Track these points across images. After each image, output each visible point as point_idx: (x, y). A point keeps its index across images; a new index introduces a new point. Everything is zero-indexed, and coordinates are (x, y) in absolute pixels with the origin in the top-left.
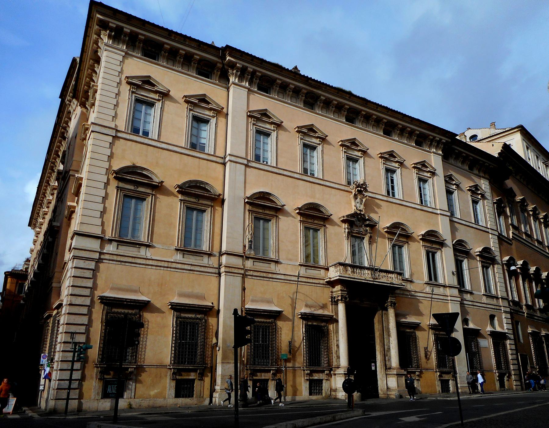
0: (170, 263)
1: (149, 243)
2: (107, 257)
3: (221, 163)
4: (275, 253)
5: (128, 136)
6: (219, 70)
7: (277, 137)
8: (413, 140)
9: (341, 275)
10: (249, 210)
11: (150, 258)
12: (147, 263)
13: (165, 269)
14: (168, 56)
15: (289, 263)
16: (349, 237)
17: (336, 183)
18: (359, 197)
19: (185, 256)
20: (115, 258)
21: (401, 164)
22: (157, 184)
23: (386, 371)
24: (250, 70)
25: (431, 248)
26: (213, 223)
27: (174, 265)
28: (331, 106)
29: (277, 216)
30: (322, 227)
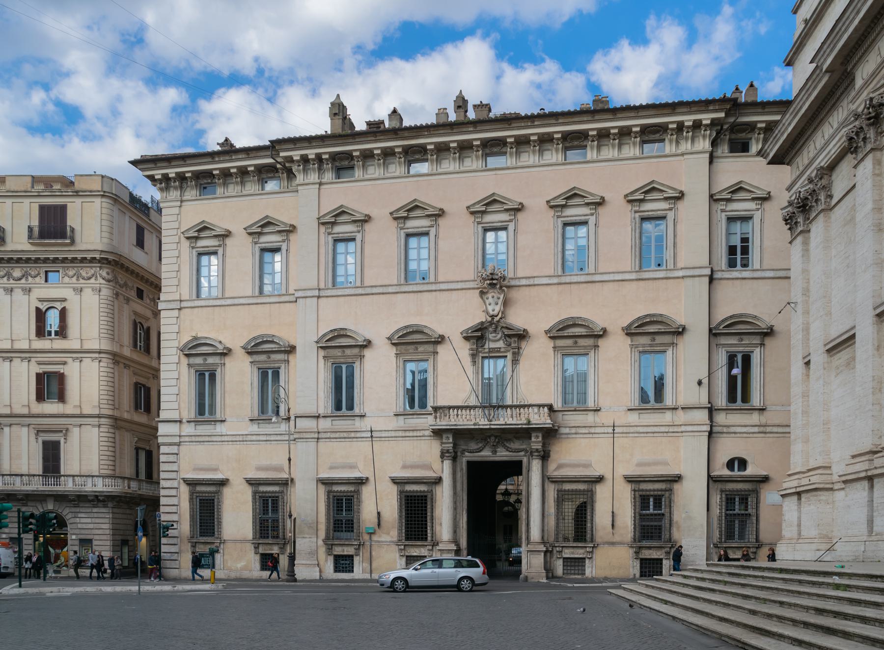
12: (223, 439)
13: (241, 443)
19: (261, 425)
20: (193, 439)
27: (249, 438)
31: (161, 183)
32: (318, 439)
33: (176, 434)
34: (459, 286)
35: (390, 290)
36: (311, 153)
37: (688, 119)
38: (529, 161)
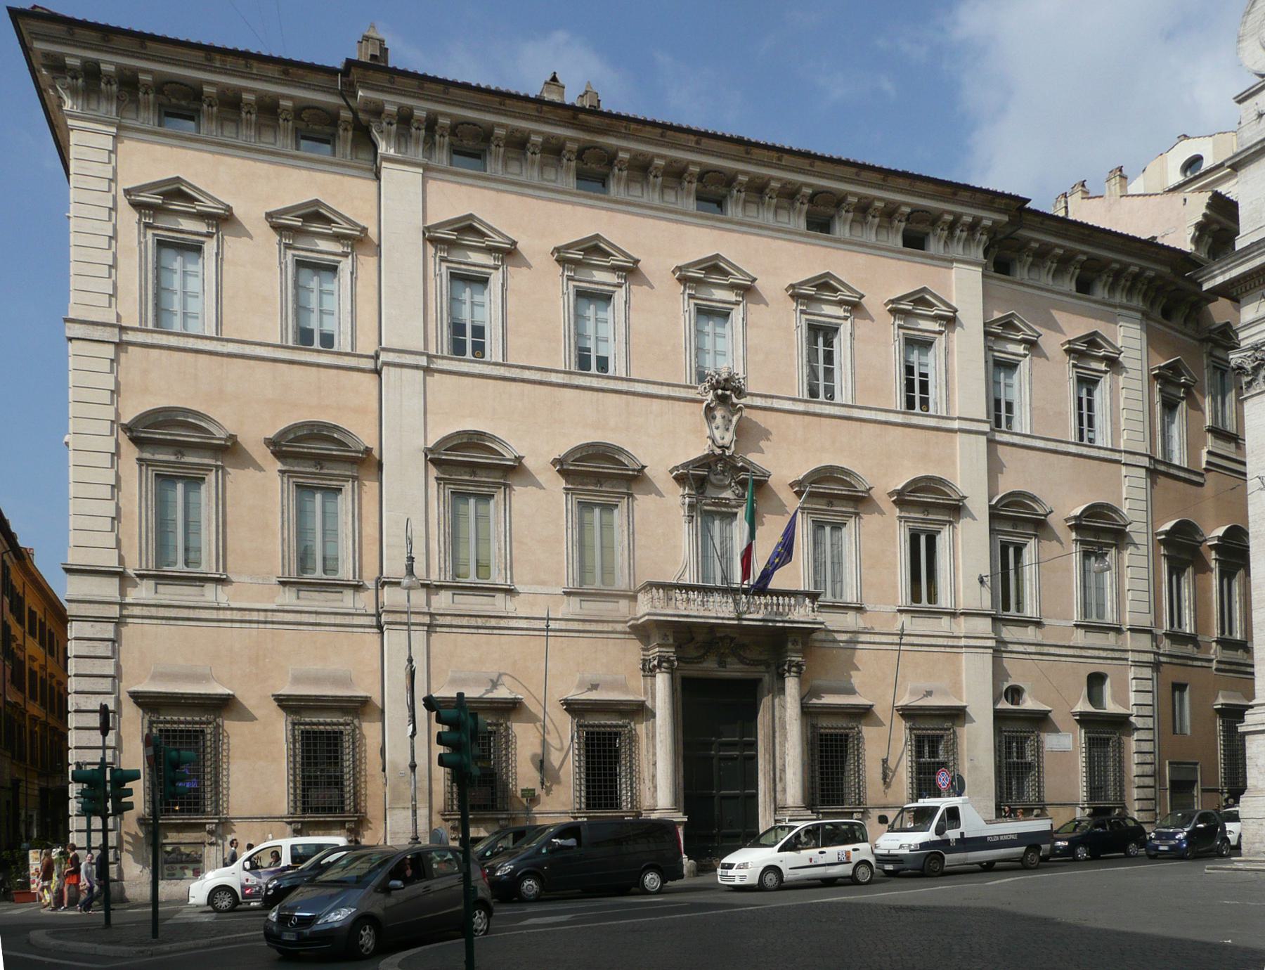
0: (271, 613)
1: (221, 575)
2: (137, 611)
3: (371, 371)
4: (503, 571)
5: (147, 338)
6: (349, 127)
7: (503, 285)
8: (897, 231)
9: (653, 611)
10: (437, 479)
11: (226, 606)
12: (220, 616)
14: (219, 112)
15: (539, 589)
16: (693, 517)
17: (662, 384)
18: (719, 413)
20: (154, 612)
21: (855, 307)
22: (223, 442)
23: (775, 814)
24: (420, 114)
25: (924, 521)
26: (358, 517)
28: (651, 173)
29: (506, 486)
30: (624, 498)
31: (75, 77)
32: (429, 626)
33: (113, 599)
34: (664, 391)
35: (554, 378)
36: (421, 108)
37: (968, 214)
38: (642, 197)
